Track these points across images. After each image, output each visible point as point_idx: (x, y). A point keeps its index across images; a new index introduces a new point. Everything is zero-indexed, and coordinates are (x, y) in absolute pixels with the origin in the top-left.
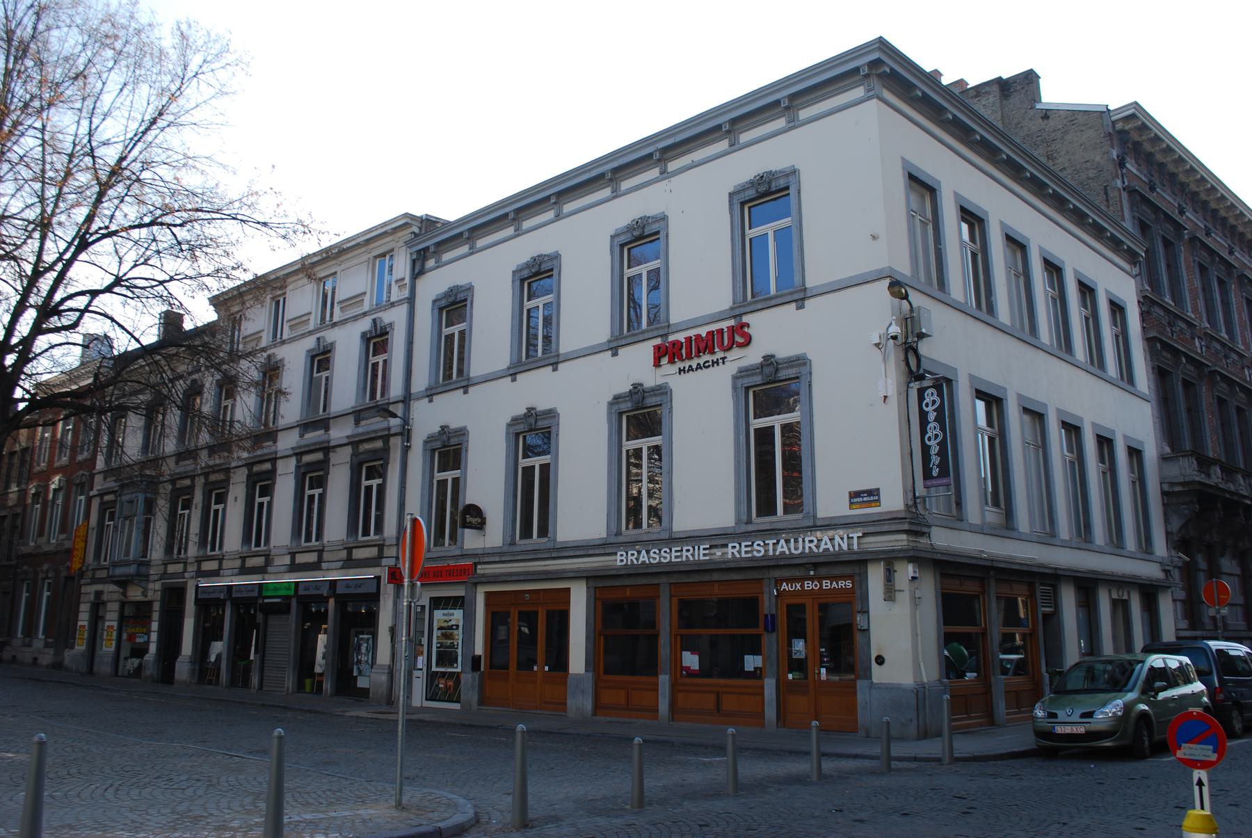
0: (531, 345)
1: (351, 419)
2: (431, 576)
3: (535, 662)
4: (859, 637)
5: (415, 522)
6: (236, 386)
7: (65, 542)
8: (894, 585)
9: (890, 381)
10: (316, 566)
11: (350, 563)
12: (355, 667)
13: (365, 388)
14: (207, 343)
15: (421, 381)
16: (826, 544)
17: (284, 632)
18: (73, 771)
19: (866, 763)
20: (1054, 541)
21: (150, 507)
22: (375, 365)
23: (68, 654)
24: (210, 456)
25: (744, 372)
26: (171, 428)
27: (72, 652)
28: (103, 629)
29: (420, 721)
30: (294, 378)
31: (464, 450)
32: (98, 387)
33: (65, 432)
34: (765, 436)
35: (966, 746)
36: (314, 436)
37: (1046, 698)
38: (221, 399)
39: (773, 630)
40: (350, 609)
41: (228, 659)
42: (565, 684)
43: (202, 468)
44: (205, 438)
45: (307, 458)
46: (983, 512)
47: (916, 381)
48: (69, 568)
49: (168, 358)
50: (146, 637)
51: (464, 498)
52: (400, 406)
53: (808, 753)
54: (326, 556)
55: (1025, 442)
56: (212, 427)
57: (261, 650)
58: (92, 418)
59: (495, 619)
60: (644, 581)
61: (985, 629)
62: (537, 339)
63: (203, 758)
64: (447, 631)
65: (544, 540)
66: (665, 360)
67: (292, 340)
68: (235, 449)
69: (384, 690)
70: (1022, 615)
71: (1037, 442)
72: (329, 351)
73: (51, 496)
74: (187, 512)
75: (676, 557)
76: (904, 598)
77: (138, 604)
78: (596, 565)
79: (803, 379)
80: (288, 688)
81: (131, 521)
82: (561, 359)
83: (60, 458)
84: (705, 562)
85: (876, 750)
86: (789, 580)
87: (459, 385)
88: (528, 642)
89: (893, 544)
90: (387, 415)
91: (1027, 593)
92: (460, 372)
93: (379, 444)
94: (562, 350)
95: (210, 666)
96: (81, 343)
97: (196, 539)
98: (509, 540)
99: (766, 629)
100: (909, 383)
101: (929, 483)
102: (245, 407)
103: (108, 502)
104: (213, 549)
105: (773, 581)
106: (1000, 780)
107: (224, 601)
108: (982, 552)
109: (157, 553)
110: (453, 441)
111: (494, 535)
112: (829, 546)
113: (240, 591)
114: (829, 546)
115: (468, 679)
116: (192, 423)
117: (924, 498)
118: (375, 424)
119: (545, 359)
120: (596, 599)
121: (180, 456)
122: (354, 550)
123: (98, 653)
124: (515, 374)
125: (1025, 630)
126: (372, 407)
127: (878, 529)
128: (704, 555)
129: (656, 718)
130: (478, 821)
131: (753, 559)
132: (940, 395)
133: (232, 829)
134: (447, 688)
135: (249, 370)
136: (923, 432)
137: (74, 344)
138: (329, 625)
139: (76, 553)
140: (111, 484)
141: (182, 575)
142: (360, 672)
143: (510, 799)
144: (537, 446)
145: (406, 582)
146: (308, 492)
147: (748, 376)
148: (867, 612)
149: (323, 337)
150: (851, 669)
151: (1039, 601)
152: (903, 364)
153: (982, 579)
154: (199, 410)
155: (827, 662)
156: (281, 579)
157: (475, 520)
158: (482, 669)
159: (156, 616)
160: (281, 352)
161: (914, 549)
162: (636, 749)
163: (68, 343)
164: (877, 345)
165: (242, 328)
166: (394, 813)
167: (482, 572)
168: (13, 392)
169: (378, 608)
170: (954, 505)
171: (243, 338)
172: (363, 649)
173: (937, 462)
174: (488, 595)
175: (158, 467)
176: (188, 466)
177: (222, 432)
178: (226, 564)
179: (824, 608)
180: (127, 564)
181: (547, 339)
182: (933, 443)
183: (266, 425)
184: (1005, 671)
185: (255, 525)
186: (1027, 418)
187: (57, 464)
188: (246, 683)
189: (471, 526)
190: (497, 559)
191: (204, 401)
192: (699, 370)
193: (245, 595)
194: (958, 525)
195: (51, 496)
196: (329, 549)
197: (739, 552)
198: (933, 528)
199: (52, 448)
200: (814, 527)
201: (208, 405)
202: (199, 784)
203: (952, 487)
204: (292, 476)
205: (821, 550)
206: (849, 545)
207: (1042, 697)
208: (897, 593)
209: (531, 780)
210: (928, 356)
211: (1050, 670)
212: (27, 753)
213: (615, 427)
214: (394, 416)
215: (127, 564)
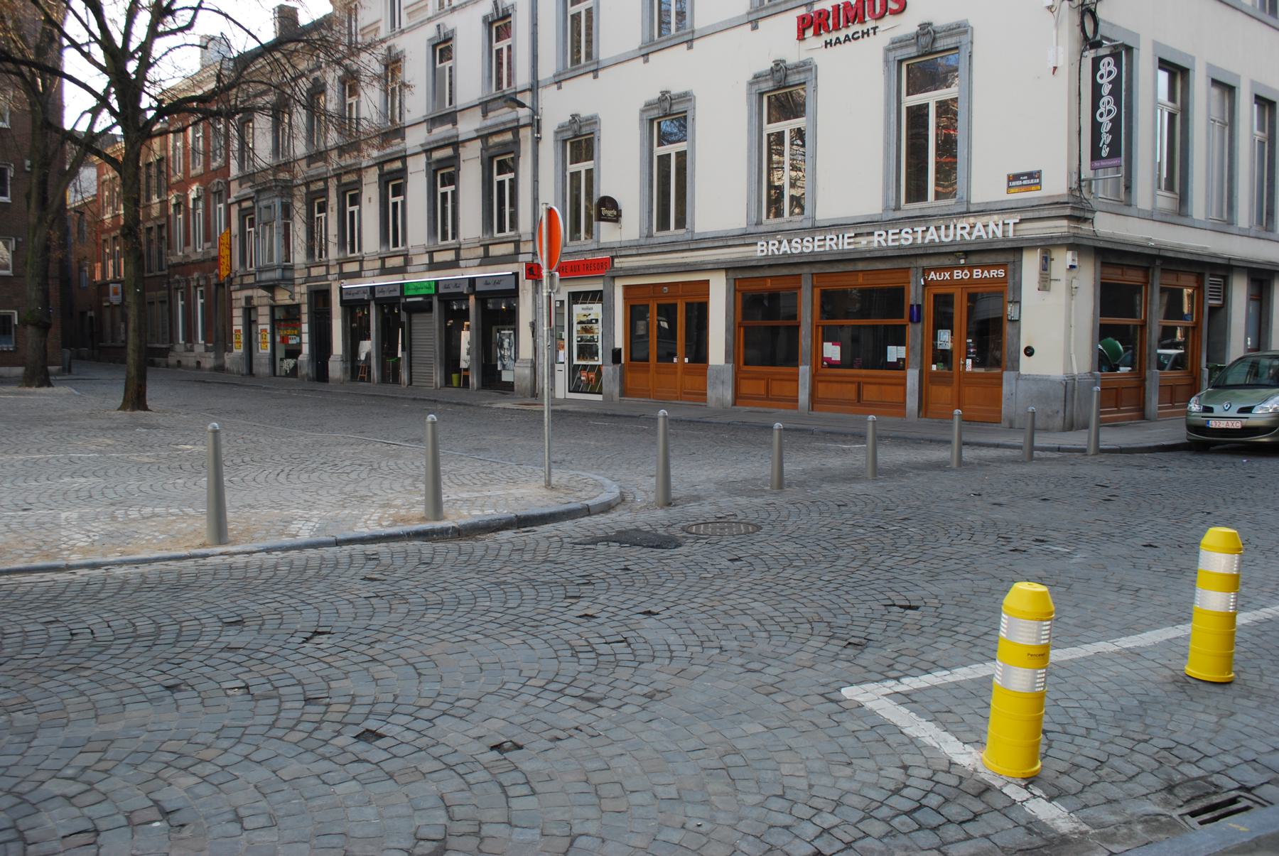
0: (664, 23)
1: (478, 111)
2: (570, 271)
3: (675, 355)
4: (1008, 328)
5: (550, 212)
6: (359, 81)
7: (212, 250)
8: (1050, 274)
9: (1061, 49)
10: (454, 264)
11: (487, 260)
12: (499, 363)
13: (491, 77)
14: (324, 37)
15: (547, 70)
16: (979, 231)
17: (428, 330)
18: (247, 459)
19: (1008, 452)
20: (1231, 229)
21: (287, 211)
22: (499, 52)
23: (228, 358)
24: (340, 156)
25: (898, 44)
26: (298, 128)
27: (231, 355)
28: (257, 333)
29: (564, 411)
30: (416, 70)
31: (596, 139)
32: (221, 91)
33: (196, 139)
34: (917, 116)
35: (1112, 438)
36: (442, 131)
37: (1203, 392)
38: (344, 95)
39: (918, 321)
40: (490, 306)
41: (377, 357)
42: (705, 375)
43: (333, 170)
44: (333, 138)
45: (437, 155)
46: (1154, 196)
47: (1091, 48)
48: (218, 276)
49: (289, 56)
50: (298, 339)
51: (599, 189)
52: (528, 94)
53: (949, 442)
54: (463, 254)
55: (1211, 120)
56: (340, 125)
57: (408, 348)
58: (220, 123)
59: (635, 313)
60: (785, 271)
61: (1145, 321)
62: (670, 16)
63: (363, 446)
64: (587, 325)
65: (682, 231)
66: (809, 33)
67: (412, 28)
68: (364, 146)
69: (527, 383)
70: (1186, 311)
71: (1224, 119)
72: (451, 39)
73: (191, 206)
74: (323, 215)
75: (819, 246)
76: (1059, 289)
77: (287, 308)
79: (963, 49)
80: (436, 384)
81: (271, 228)
82: (696, 36)
83: (194, 168)
84: (850, 252)
85: (1019, 440)
86: (937, 269)
87: (588, 69)
88: (668, 336)
89: (1052, 231)
90: (515, 105)
91: (1195, 285)
92: (589, 55)
93: (508, 137)
94: (698, 26)
95: (361, 364)
96: (198, 43)
97: (336, 240)
98: (646, 232)
99: (911, 320)
100: (1083, 51)
101: (1097, 164)
102: (370, 104)
103: (246, 209)
104: (353, 251)
105: (921, 271)
106: (1145, 471)
107: (368, 301)
108: (1150, 239)
109: (299, 257)
110: (585, 131)
111: (631, 227)
112: (983, 233)
113: (383, 291)
114: (983, 233)
115: (609, 371)
116: (319, 121)
117: (1090, 182)
118: (503, 115)
119: (679, 36)
120: (735, 290)
121: (311, 159)
122: (491, 247)
123: (255, 355)
124: (648, 54)
125: (1188, 323)
126: (500, 98)
127: (1036, 215)
128: (849, 244)
129: (796, 408)
130: (623, 500)
131: (900, 248)
132: (1118, 64)
133: (395, 507)
134: (589, 381)
135: (370, 63)
136: (1095, 107)
137: (193, 45)
138: (472, 321)
139: (222, 260)
140: (247, 190)
141: (325, 277)
142: (504, 366)
143: (653, 480)
144: (671, 134)
145: (545, 272)
146: (441, 190)
147: (901, 47)
148: (1019, 302)
149: (443, 24)
150: (998, 363)
151: (1207, 293)
152: (1078, 30)
153: (1146, 270)
154: (325, 109)
155: (974, 353)
156: (420, 278)
157: (610, 213)
158: (623, 361)
159: (305, 318)
160: (401, 43)
161: (1074, 236)
162: (776, 434)
163: (186, 45)
164: (1050, 8)
165: (359, 17)
166: (545, 492)
167: (619, 265)
168: (139, 100)
169: (518, 304)
170: (1123, 189)
171: (361, 30)
172: (506, 345)
173: (1108, 141)
174: (627, 289)
175: (290, 171)
176: (319, 168)
177: (350, 130)
178: (366, 265)
179: (973, 298)
180: (272, 269)
181: (681, 15)
182: (1105, 81)
183: (393, 121)
184: (1161, 366)
185: (392, 226)
186: (1215, 92)
187: (193, 173)
188: (396, 379)
189: (607, 219)
190: (634, 252)
191: (328, 98)
192: (847, 43)
193: (387, 295)
194: (1126, 210)
195: (191, 206)
196: (466, 246)
197: (886, 241)
198: (1098, 214)
199: (186, 155)
200: (967, 213)
201: (333, 102)
202: (362, 468)
203: (1123, 169)
204: (424, 174)
205: (973, 237)
206: (1003, 232)
207: (1199, 391)
208: (1053, 283)
209: (673, 463)
210: (1106, 19)
211: (1210, 365)
212: (203, 444)
213: (755, 108)
214: (523, 105)
215: (272, 269)
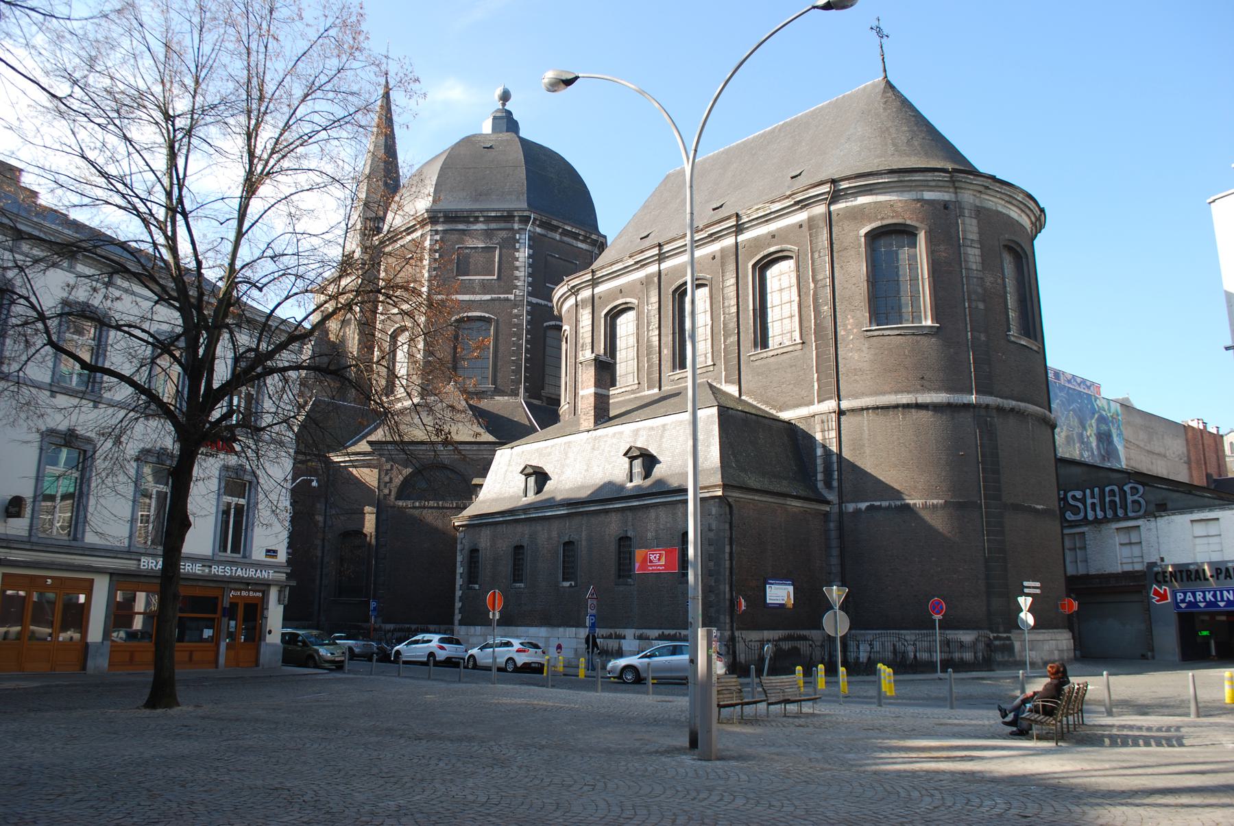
25: (226, 468)
78: (48, 559)
86: (236, 590)
